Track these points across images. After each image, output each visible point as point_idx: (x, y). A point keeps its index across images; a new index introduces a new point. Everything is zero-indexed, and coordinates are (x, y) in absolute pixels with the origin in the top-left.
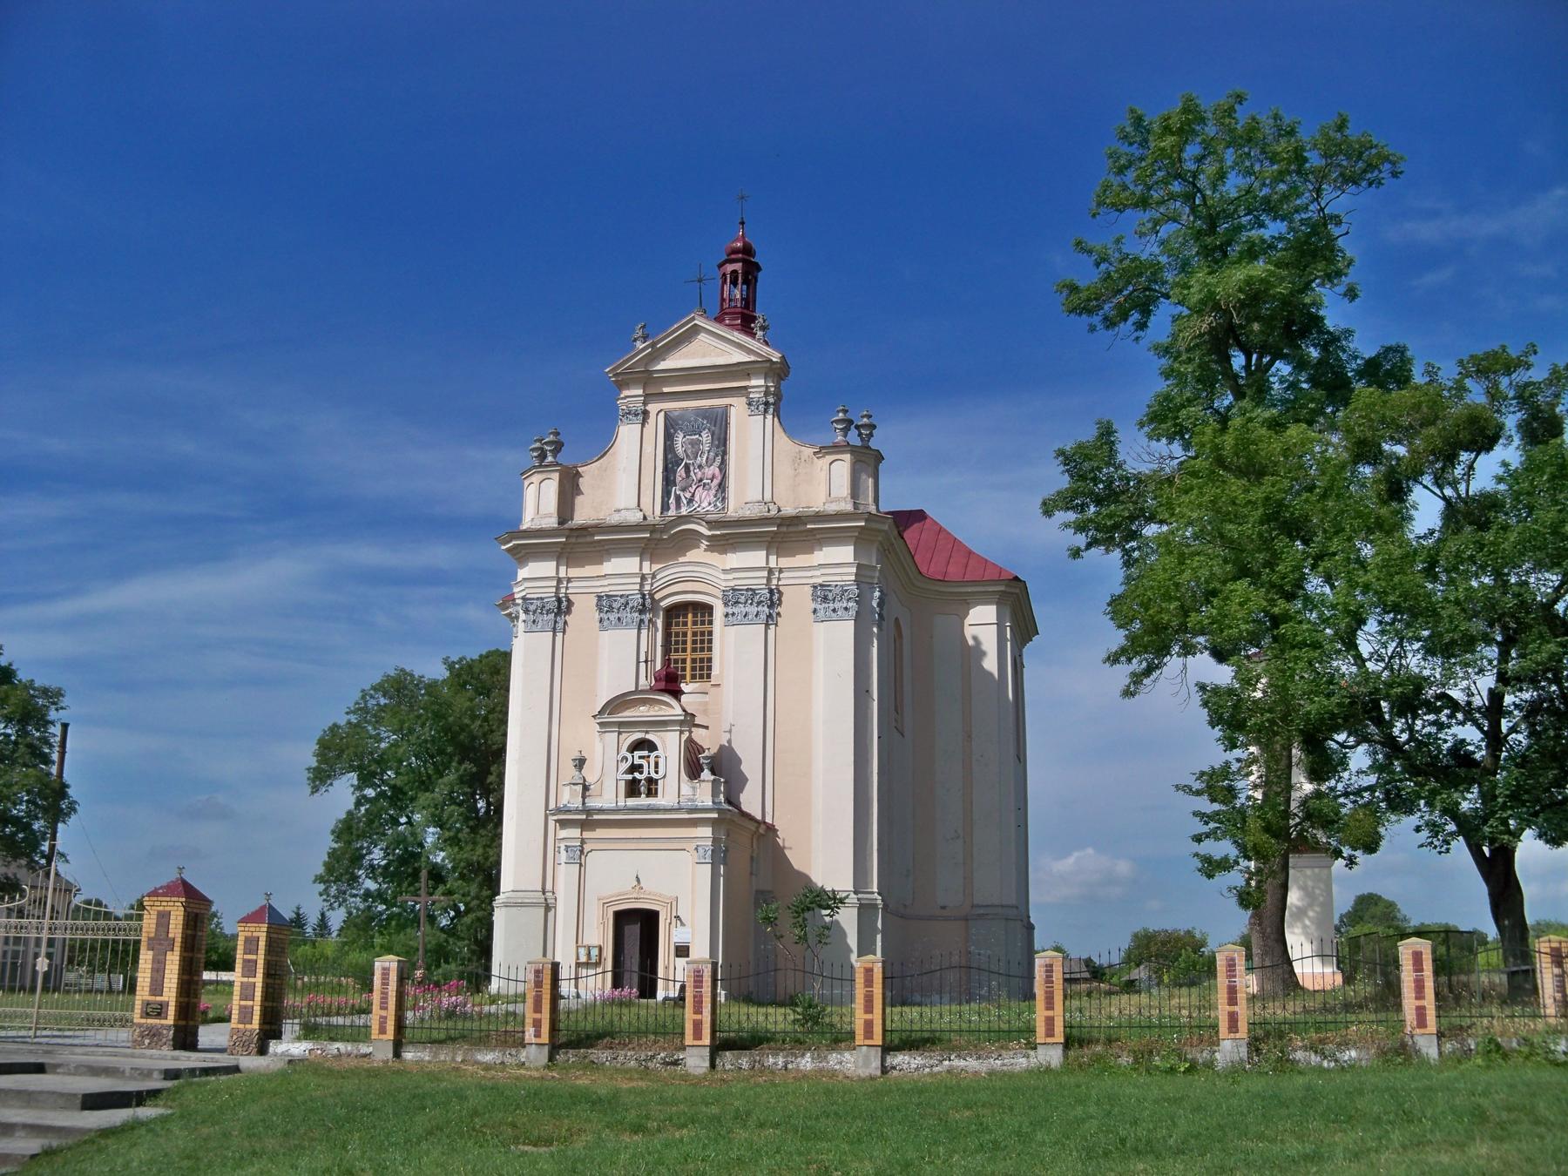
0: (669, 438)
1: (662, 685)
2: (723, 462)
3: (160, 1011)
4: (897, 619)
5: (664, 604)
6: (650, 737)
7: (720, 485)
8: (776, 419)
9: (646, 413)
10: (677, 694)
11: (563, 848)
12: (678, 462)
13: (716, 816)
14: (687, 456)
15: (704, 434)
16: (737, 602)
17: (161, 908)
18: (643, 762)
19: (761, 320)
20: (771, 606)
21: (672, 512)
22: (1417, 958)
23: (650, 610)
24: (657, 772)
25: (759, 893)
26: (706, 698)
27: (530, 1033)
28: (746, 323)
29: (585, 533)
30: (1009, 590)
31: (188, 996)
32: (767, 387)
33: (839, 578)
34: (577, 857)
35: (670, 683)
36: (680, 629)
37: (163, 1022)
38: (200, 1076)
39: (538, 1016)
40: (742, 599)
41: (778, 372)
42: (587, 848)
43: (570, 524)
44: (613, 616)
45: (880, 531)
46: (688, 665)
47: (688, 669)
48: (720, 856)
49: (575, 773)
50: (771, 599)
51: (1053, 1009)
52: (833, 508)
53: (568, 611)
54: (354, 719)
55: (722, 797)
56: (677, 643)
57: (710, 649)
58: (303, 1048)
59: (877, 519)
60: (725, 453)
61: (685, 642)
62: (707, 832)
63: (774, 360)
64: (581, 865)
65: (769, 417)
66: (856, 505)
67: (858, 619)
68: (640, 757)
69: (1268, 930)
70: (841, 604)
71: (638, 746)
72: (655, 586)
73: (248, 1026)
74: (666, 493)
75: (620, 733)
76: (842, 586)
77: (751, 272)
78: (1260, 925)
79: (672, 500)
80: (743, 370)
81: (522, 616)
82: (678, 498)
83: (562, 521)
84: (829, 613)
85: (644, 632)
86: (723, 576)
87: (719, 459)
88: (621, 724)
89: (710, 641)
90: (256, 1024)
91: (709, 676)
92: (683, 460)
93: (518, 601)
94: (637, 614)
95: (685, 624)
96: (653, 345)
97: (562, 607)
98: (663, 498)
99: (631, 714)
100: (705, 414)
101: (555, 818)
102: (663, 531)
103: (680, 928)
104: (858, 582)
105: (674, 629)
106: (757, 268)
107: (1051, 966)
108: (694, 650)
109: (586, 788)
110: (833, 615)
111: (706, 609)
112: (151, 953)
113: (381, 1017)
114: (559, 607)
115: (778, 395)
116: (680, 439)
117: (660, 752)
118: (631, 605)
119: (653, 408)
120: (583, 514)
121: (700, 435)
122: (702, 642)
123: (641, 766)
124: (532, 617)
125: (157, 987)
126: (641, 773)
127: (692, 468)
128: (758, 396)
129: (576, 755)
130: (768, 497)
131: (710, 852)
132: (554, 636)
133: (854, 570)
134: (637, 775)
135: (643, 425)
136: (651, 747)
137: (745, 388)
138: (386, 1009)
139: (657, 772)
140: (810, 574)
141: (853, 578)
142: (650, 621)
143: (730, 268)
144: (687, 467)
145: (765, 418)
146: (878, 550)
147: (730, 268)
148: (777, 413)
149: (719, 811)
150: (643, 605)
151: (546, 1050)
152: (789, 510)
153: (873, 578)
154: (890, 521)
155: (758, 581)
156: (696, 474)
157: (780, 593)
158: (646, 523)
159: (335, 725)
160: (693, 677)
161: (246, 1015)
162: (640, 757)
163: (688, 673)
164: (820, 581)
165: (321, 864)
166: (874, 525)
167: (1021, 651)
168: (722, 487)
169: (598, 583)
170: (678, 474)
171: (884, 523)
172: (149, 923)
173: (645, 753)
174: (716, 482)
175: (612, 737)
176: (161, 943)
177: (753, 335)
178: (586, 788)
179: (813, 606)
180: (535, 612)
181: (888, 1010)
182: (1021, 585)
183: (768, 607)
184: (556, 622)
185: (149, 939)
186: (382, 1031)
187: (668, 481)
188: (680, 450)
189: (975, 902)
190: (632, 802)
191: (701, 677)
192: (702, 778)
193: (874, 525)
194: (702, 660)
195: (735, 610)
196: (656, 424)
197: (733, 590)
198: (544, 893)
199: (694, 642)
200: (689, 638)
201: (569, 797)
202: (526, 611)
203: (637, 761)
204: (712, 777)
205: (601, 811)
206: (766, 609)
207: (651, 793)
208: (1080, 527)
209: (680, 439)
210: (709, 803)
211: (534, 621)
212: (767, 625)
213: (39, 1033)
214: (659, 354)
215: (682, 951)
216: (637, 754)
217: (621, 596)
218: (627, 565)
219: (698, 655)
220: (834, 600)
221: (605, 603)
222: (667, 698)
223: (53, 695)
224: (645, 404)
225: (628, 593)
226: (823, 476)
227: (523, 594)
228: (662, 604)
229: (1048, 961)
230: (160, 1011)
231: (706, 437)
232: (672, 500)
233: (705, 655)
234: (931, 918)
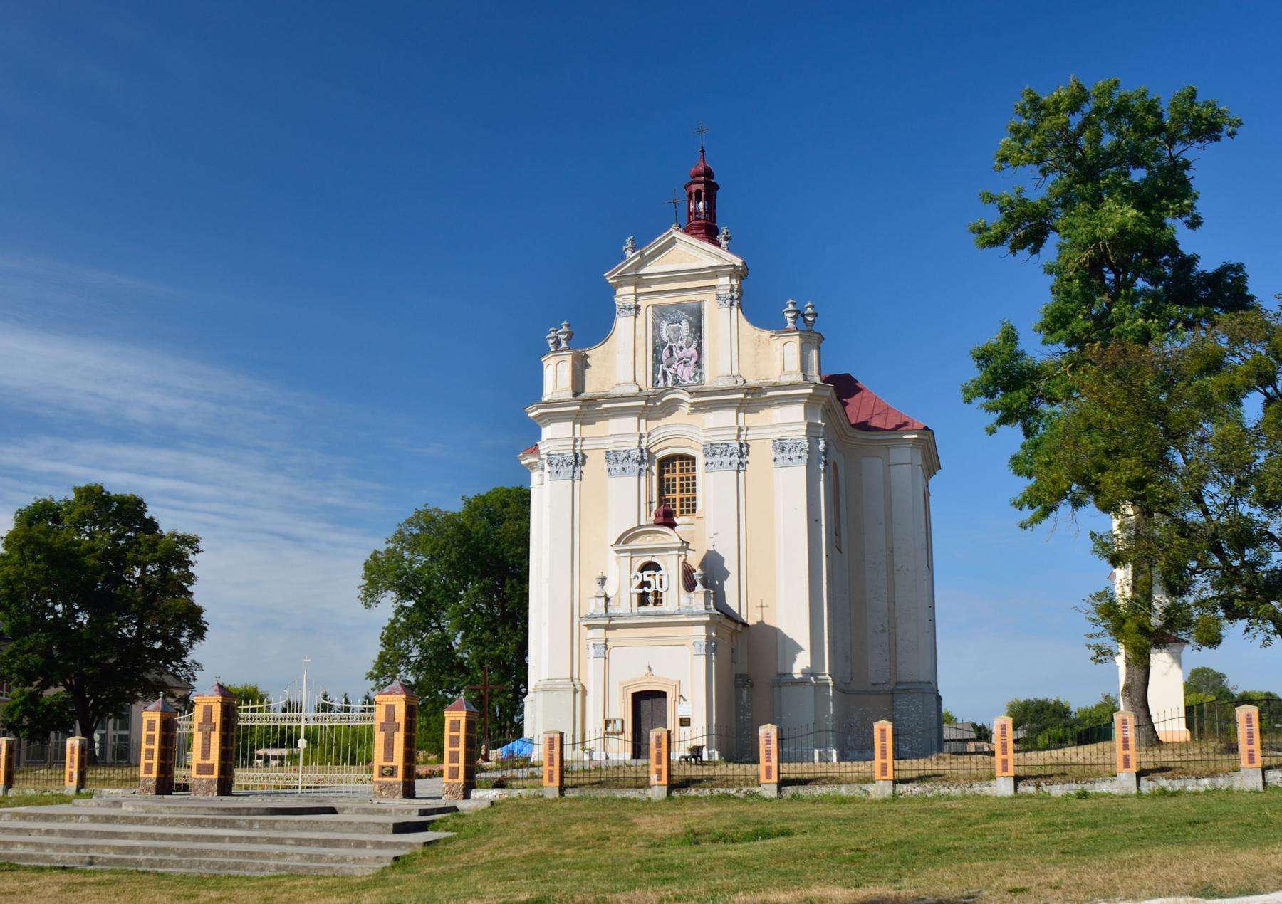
0: (656, 327)
1: (661, 520)
2: (700, 345)
3: (393, 773)
4: (834, 462)
5: (659, 455)
6: (654, 560)
7: (697, 363)
8: (739, 310)
9: (637, 308)
10: (672, 525)
11: (591, 646)
13: (708, 619)
14: (670, 340)
16: (714, 454)
17: (388, 703)
19: (725, 232)
20: (741, 456)
21: (661, 384)
22: (1249, 719)
23: (647, 462)
24: (661, 587)
25: (738, 676)
26: (693, 528)
27: (654, 778)
28: (710, 233)
29: (593, 402)
30: (922, 437)
31: (409, 762)
32: (732, 286)
34: (603, 653)
35: (667, 519)
36: (671, 476)
37: (395, 779)
38: (1047, 748)
39: (659, 767)
40: (718, 451)
41: (741, 274)
42: (610, 645)
43: (582, 396)
44: (619, 467)
45: (823, 396)
46: (678, 503)
47: (678, 506)
48: (712, 647)
49: (598, 588)
50: (741, 451)
51: (1006, 754)
52: (786, 380)
53: (584, 462)
54: (391, 546)
55: (712, 606)
56: (668, 485)
57: (694, 490)
58: (494, 794)
59: (821, 387)
60: (701, 337)
62: (701, 630)
63: (737, 264)
64: (605, 658)
65: (734, 309)
66: (805, 378)
67: (810, 466)
69: (1136, 700)
70: (795, 454)
71: (647, 567)
72: (650, 442)
73: (456, 781)
74: (655, 371)
75: (632, 557)
77: (711, 192)
78: (1129, 696)
80: (712, 273)
81: (547, 468)
82: (665, 374)
83: (576, 394)
84: (787, 460)
85: (643, 479)
86: (703, 434)
87: (695, 343)
88: (632, 551)
89: (694, 484)
90: (461, 778)
91: (694, 511)
92: (667, 343)
93: (542, 457)
94: (637, 465)
95: (674, 471)
96: (641, 254)
97: (579, 460)
98: (653, 374)
99: (642, 543)
100: (681, 306)
101: (585, 623)
102: (654, 401)
103: (684, 704)
104: (808, 436)
105: (666, 476)
106: (716, 187)
107: (1005, 725)
108: (682, 491)
109: (607, 600)
110: (790, 462)
111: (688, 460)
112: (383, 733)
113: (550, 771)
114: (576, 461)
115: (740, 291)
116: (664, 327)
118: (632, 458)
119: (643, 302)
120: (591, 390)
122: (688, 485)
124: (555, 469)
125: (389, 754)
126: (649, 587)
127: (674, 349)
128: (724, 292)
129: (599, 575)
130: (735, 372)
131: (704, 646)
132: (573, 481)
133: (805, 427)
134: (646, 589)
135: (636, 317)
136: (655, 567)
137: (714, 287)
138: (553, 765)
139: (661, 587)
140: (770, 431)
141: (804, 433)
142: (648, 469)
143: (695, 187)
144: (670, 349)
145: (731, 309)
146: (822, 410)
147: (695, 187)
148: (740, 306)
149: (711, 615)
150: (642, 458)
151: (666, 788)
152: (752, 382)
153: (819, 433)
154: (831, 389)
155: (730, 437)
156: (677, 354)
157: (748, 446)
158: (642, 394)
159: (376, 552)
160: (682, 512)
161: (454, 774)
162: (648, 576)
163: (678, 509)
164: (779, 436)
166: (819, 393)
167: (928, 483)
168: (698, 364)
169: (606, 441)
170: (664, 355)
171: (827, 390)
172: (380, 714)
173: (652, 572)
174: (694, 360)
175: (626, 560)
176: (389, 727)
177: (719, 245)
178: (607, 600)
179: (774, 455)
180: (557, 465)
181: (781, 765)
182: (930, 433)
183: (739, 457)
184: (574, 472)
185: (200, 724)
186: (551, 780)
187: (657, 360)
189: (899, 680)
190: (643, 609)
191: (688, 511)
192: (696, 590)
193: (819, 393)
194: (688, 499)
195: (713, 460)
196: (646, 316)
197: (712, 444)
198: (572, 681)
199: (682, 485)
200: (678, 482)
201: (596, 607)
202: (551, 464)
203: (646, 579)
204: (705, 590)
205: (619, 616)
206: (737, 458)
207: (658, 601)
208: (991, 409)
210: (702, 608)
211: (557, 472)
212: (738, 471)
213: (303, 790)
214: (643, 262)
215: (685, 722)
216: (646, 573)
217: (624, 451)
218: (629, 425)
219: (685, 495)
220: (789, 451)
221: (612, 457)
222: (666, 530)
223: (192, 542)
224: (636, 300)
226: (778, 354)
227: (548, 451)
228: (657, 455)
229: (1003, 723)
230: (393, 773)
231: (685, 325)
233: (690, 495)
234: (866, 692)
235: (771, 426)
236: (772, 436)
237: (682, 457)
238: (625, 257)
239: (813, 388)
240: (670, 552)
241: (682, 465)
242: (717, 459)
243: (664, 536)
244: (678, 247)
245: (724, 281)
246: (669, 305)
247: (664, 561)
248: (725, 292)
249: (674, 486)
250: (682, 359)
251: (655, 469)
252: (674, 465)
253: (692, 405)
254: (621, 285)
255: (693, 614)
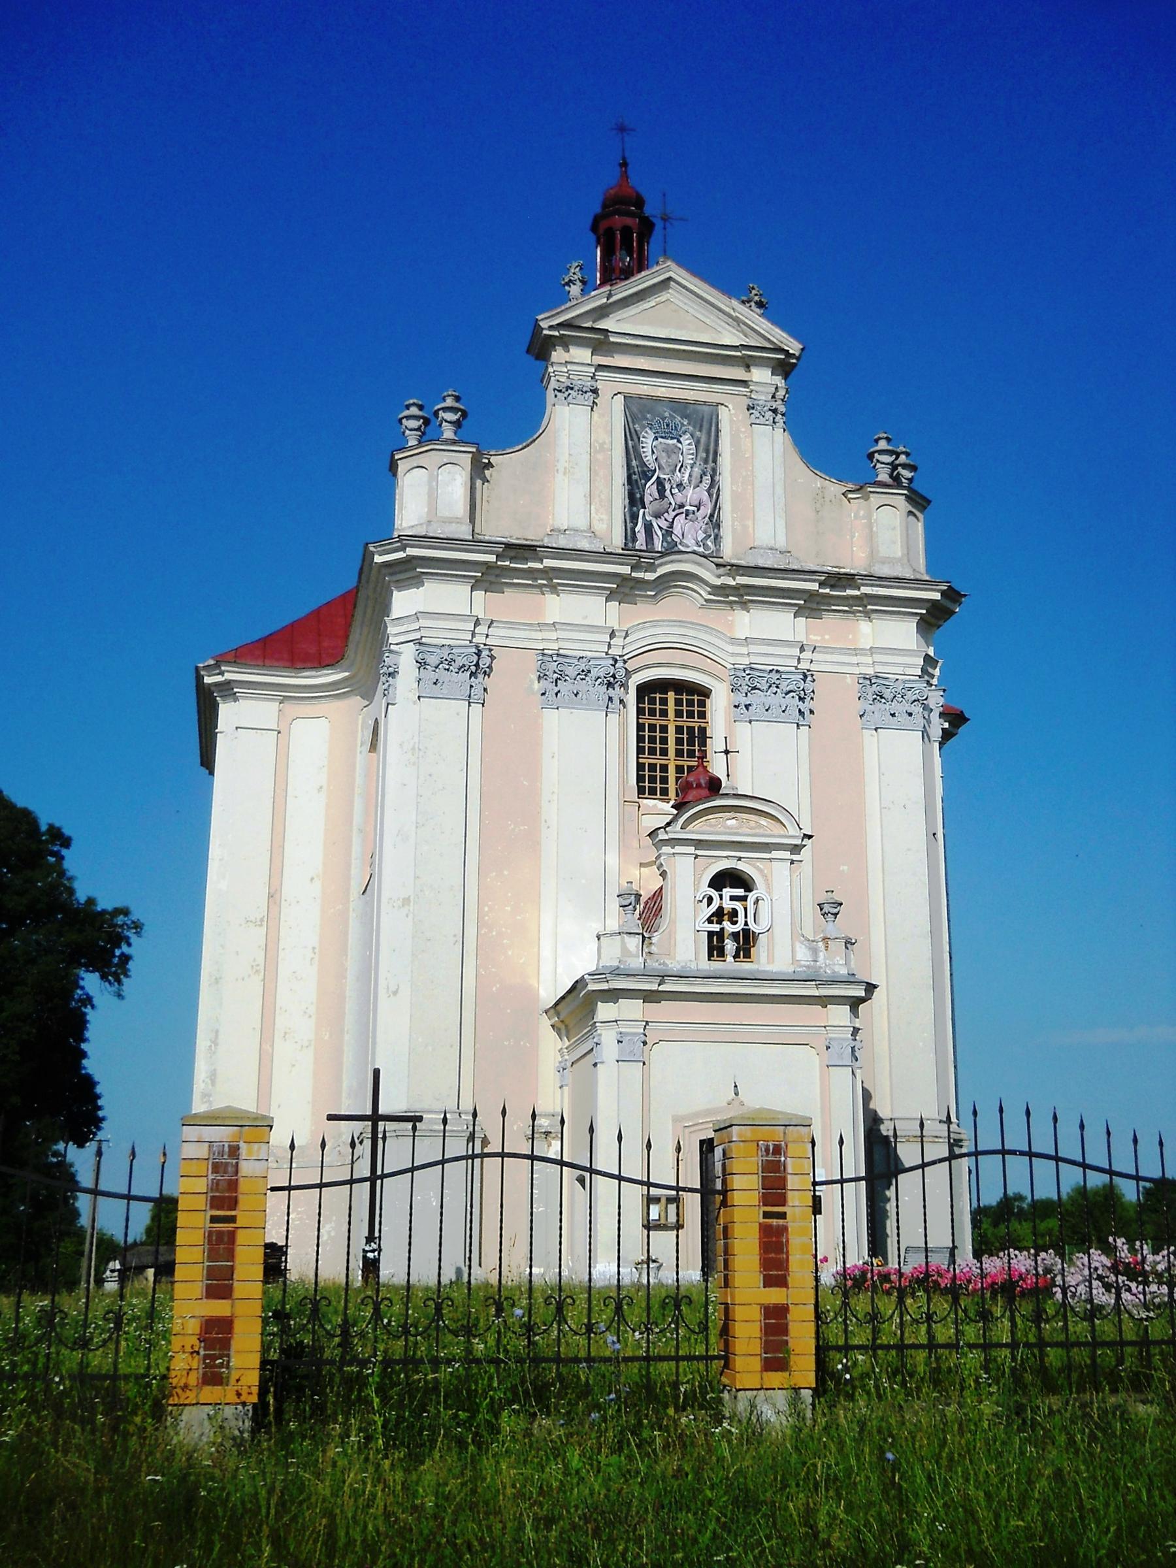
0: (632, 438)
12: (646, 475)
15: (686, 440)
18: (738, 906)
29: (527, 554)
33: (899, 670)
61: (664, 741)
68: (732, 898)
76: (905, 682)
79: (640, 527)
82: (648, 528)
87: (707, 480)
88: (699, 844)
116: (648, 440)
117: (759, 891)
121: (679, 441)
123: (734, 913)
127: (667, 486)
137: (744, 383)
140: (854, 660)
144: (660, 483)
155: (784, 658)
162: (732, 898)
164: (870, 671)
165: (89, 1053)
170: (647, 492)
179: (860, 706)
187: (635, 500)
188: (649, 459)
190: (716, 966)
191: (653, 792)
200: (671, 735)
203: (728, 905)
209: (650, 441)
214: (602, 312)
216: (728, 892)
225: (589, 654)
232: (640, 527)
235: (856, 651)
236: (857, 670)
237: (680, 686)
238: (566, 298)
239: (943, 593)
240: (775, 854)
241: (678, 702)
242: (756, 698)
243: (764, 821)
244: (670, 294)
245: (761, 375)
246: (658, 400)
247: (761, 871)
248: (763, 397)
249: (679, 742)
250: (682, 506)
251: (631, 698)
252: (664, 702)
253: (720, 590)
254: (565, 342)
255: (834, 982)
